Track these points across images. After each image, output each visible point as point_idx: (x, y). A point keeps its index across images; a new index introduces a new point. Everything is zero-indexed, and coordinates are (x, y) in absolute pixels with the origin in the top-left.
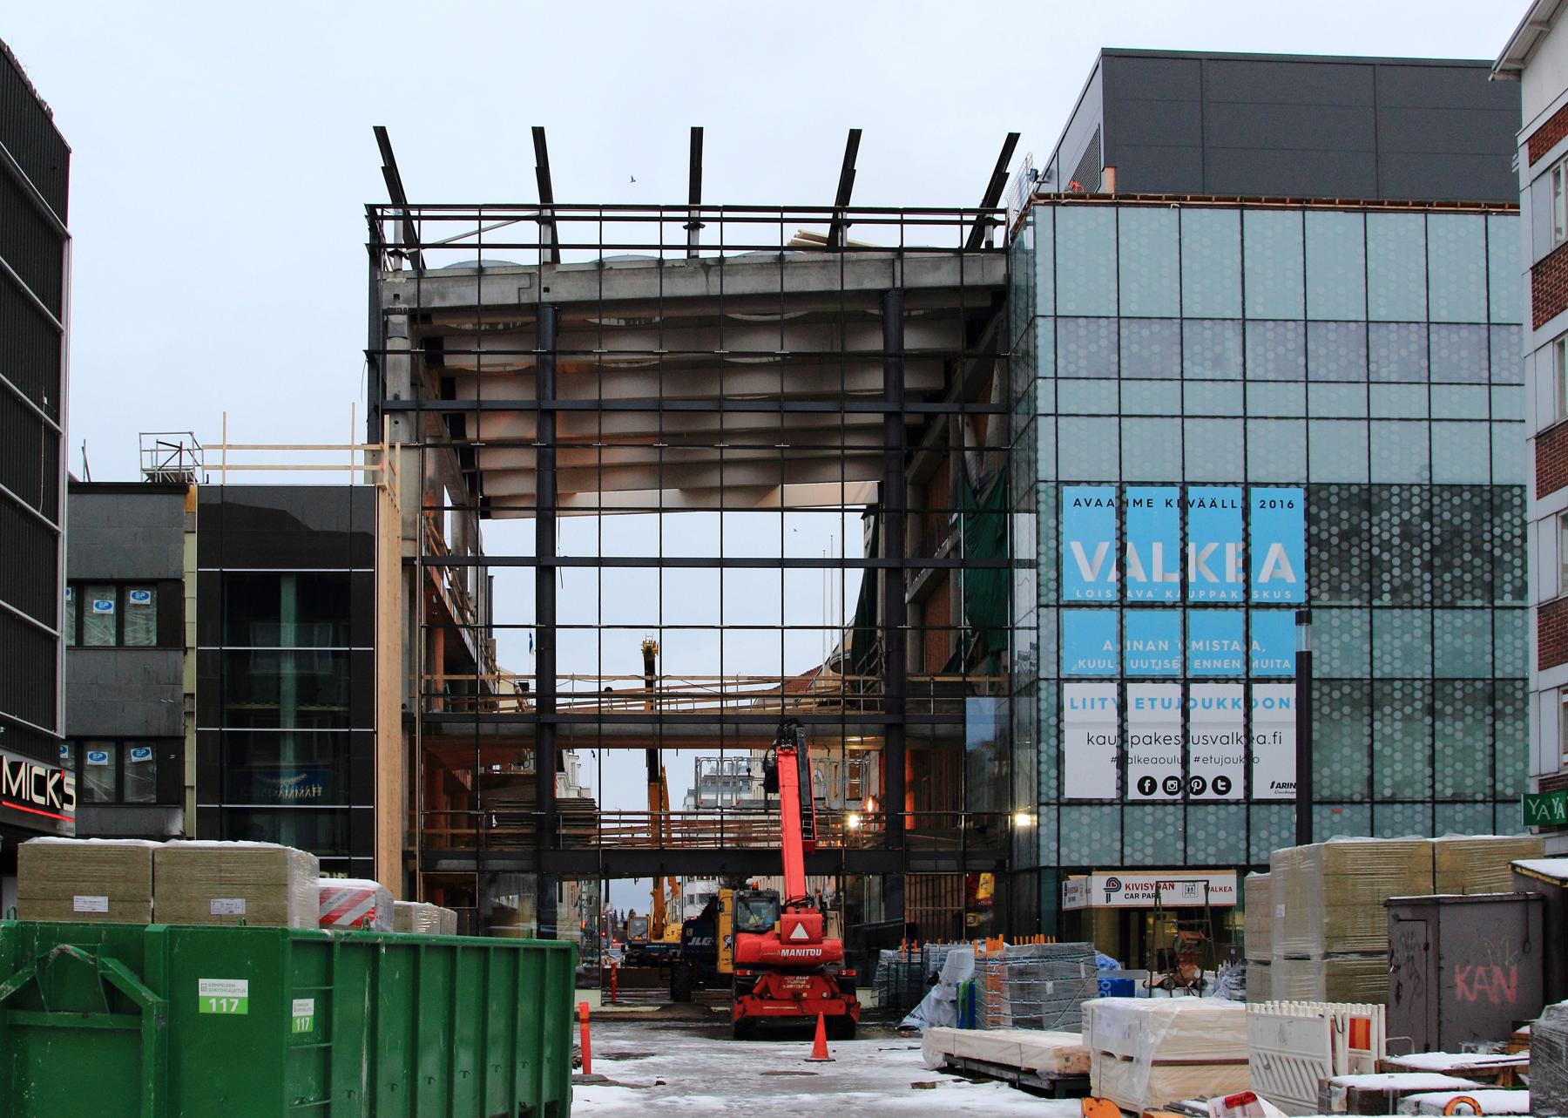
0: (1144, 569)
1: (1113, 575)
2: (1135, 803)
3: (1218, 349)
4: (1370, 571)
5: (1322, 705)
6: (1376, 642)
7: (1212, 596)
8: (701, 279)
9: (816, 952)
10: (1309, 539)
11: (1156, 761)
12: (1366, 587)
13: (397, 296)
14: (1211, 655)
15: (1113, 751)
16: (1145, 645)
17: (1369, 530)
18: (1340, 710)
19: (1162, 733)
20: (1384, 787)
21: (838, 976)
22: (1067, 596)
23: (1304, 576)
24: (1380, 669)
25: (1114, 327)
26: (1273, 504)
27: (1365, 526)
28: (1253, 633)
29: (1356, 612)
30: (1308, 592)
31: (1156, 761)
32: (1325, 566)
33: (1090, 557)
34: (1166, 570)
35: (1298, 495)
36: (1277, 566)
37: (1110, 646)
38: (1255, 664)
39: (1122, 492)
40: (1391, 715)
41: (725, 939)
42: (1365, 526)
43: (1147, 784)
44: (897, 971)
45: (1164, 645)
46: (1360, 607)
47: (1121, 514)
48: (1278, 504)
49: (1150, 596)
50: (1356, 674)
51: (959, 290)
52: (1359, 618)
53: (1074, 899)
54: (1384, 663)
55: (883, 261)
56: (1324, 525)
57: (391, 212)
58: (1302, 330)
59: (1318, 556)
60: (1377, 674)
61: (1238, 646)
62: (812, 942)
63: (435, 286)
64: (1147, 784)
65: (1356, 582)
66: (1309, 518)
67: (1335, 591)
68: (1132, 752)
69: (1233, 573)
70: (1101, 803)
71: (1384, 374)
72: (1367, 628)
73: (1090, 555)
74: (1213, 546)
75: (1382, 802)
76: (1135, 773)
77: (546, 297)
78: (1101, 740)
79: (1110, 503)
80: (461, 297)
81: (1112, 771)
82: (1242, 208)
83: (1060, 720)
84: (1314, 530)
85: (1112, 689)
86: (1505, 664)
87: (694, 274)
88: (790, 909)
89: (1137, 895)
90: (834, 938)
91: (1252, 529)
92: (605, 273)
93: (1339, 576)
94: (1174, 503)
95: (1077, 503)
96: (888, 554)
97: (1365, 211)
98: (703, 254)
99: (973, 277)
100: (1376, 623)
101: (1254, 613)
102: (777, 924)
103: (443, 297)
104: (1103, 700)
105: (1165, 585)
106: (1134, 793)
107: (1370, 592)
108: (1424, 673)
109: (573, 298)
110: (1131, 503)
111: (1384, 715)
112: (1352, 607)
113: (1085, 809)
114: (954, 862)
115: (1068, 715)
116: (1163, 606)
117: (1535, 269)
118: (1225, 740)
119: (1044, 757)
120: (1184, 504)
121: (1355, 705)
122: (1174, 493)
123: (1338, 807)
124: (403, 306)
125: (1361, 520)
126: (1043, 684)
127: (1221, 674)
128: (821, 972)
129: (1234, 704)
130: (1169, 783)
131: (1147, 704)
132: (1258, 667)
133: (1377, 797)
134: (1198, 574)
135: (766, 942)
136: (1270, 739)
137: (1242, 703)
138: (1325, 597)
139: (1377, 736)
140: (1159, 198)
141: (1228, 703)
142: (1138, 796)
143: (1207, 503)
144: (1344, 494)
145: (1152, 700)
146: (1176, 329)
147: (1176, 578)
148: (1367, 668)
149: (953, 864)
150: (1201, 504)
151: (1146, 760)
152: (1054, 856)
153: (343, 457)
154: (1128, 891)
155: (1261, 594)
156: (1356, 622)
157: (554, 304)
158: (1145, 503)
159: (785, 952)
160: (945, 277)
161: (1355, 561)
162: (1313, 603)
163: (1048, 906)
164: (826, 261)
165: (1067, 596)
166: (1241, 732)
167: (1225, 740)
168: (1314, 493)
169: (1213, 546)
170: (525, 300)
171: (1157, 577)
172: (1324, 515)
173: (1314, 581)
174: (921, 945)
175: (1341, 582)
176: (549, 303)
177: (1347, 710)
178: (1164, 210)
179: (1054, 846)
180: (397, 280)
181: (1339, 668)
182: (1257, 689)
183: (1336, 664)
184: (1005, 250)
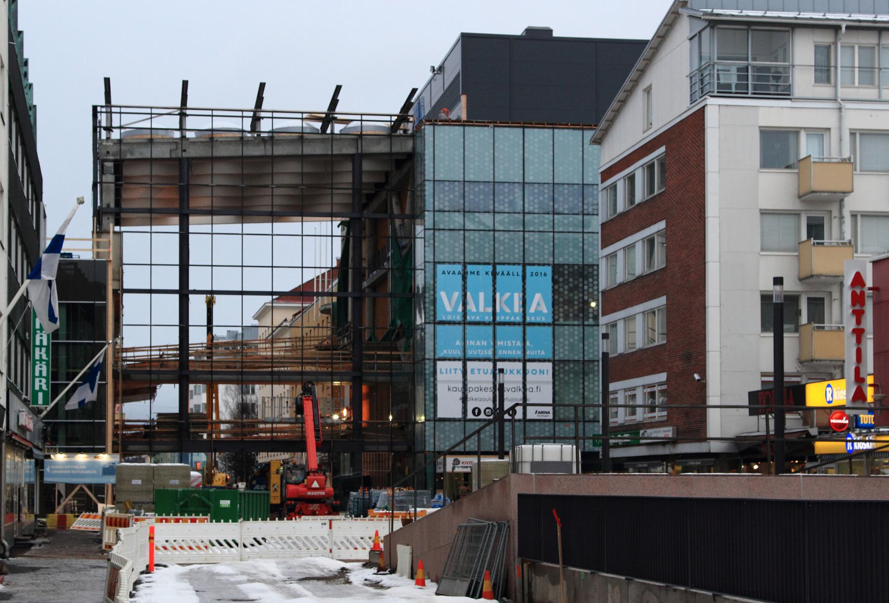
0: (475, 303)
1: (460, 309)
2: (471, 420)
3: (511, 198)
4: (583, 307)
5: (560, 373)
6: (586, 342)
7: (507, 319)
8: (262, 147)
9: (322, 493)
10: (554, 291)
11: (481, 400)
12: (581, 315)
13: (108, 152)
14: (507, 348)
15: (460, 395)
16: (476, 343)
17: (583, 287)
18: (568, 376)
19: (483, 386)
20: (590, 414)
21: (332, 504)
22: (438, 319)
23: (551, 309)
24: (588, 356)
25: (462, 186)
26: (537, 274)
27: (581, 285)
28: (527, 337)
29: (576, 328)
30: (553, 317)
31: (481, 400)
32: (561, 305)
33: (449, 299)
34: (486, 306)
35: (549, 270)
36: (538, 305)
37: (459, 343)
38: (528, 353)
39: (465, 267)
40: (593, 378)
41: (273, 486)
42: (581, 285)
43: (476, 411)
44: (358, 502)
45: (484, 343)
46: (578, 325)
47: (464, 278)
48: (539, 274)
49: (478, 319)
50: (576, 358)
51: (390, 154)
52: (577, 331)
54: (589, 353)
55: (353, 139)
56: (561, 285)
57: (104, 110)
58: (551, 189)
59: (558, 300)
60: (586, 358)
61: (519, 344)
62: (321, 488)
63: (128, 147)
64: (476, 411)
65: (576, 313)
66: (554, 281)
67: (566, 317)
68: (469, 395)
69: (517, 308)
70: (454, 420)
72: (581, 335)
73: (449, 299)
74: (508, 295)
75: (589, 421)
76: (471, 406)
77: (185, 155)
78: (455, 389)
79: (459, 273)
80: (141, 154)
81: (460, 404)
82: (524, 127)
83: (435, 379)
84: (556, 287)
85: (459, 364)
87: (258, 144)
88: (311, 474)
90: (329, 486)
91: (527, 286)
92: (214, 143)
94: (490, 273)
95: (444, 273)
96: (353, 290)
97: (583, 129)
98: (262, 135)
99: (396, 149)
100: (586, 333)
101: (528, 328)
102: (306, 480)
103: (132, 153)
104: (456, 370)
105: (485, 313)
106: (470, 416)
107: (583, 318)
109: (198, 156)
110: (469, 273)
111: (589, 379)
112: (574, 325)
113: (447, 423)
114: (386, 447)
115: (439, 376)
116: (484, 324)
117: (602, 225)
118: (513, 390)
119: (427, 397)
120: (494, 274)
121: (576, 374)
122: (490, 268)
123: (568, 423)
124: (111, 158)
125: (579, 282)
126: (427, 362)
127: (512, 357)
128: (324, 502)
129: (518, 372)
130: (487, 410)
131: (476, 371)
132: (530, 354)
133: (586, 419)
134: (501, 308)
135: (301, 488)
136: (535, 389)
137: (521, 372)
139: (586, 389)
140: (484, 122)
141: (515, 372)
142: (473, 417)
143: (506, 273)
144: (571, 270)
145: (479, 370)
146: (491, 187)
147: (490, 310)
148: (581, 355)
149: (386, 448)
150: (503, 274)
151: (476, 399)
152: (432, 446)
155: (530, 318)
156: (576, 333)
157: (188, 158)
158: (476, 273)
159: (309, 493)
160: (382, 148)
161: (576, 303)
162: (557, 323)
163: (429, 470)
164: (324, 139)
165: (438, 319)
166: (521, 386)
167: (513, 390)
168: (557, 269)
169: (508, 295)
170: (174, 156)
171: (481, 309)
172: (561, 279)
173: (556, 312)
174: (369, 490)
177: (572, 376)
178: (486, 128)
179: (432, 441)
180: (108, 144)
181: (568, 355)
182: (529, 365)
184: (413, 136)
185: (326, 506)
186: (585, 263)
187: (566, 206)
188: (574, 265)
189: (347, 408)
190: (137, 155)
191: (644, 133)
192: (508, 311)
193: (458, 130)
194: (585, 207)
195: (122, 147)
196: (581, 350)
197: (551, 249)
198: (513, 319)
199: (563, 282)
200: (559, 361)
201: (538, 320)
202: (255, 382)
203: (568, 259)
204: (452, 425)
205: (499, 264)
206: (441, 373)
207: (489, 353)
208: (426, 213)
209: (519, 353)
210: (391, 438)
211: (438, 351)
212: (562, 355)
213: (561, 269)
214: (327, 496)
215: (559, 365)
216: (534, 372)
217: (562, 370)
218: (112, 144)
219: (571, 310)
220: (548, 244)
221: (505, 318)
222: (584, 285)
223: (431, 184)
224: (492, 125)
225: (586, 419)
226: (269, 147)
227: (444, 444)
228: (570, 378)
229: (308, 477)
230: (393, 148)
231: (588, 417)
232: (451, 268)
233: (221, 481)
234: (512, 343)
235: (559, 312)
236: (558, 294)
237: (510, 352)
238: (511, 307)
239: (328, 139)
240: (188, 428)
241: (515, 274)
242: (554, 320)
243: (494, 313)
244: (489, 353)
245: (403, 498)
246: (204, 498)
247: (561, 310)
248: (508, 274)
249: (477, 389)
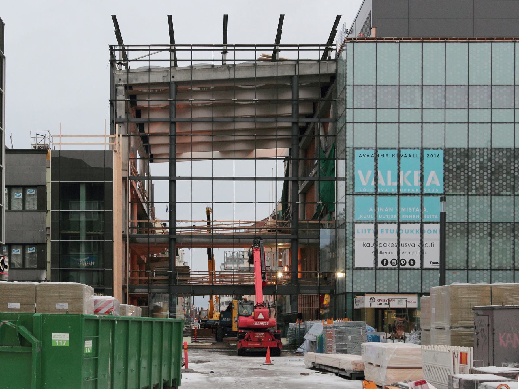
2: (380, 269)
4: (468, 181)
9: (267, 324)
10: (445, 169)
11: (388, 253)
12: (466, 187)
13: (120, 80)
15: (373, 249)
19: (390, 243)
22: (356, 191)
23: (443, 183)
24: (471, 218)
27: (466, 164)
29: (462, 197)
30: (444, 189)
31: (388, 253)
32: (451, 179)
33: (365, 176)
34: (392, 181)
35: (441, 152)
36: (433, 179)
38: (424, 217)
40: (475, 236)
43: (385, 262)
44: (295, 331)
45: (391, 209)
46: (464, 195)
47: (376, 160)
48: (434, 156)
50: (462, 221)
52: (463, 199)
53: (358, 305)
54: (472, 216)
55: (291, 65)
57: (118, 48)
58: (444, 89)
60: (470, 221)
61: (418, 210)
63: (134, 75)
64: (385, 262)
65: (462, 185)
66: (446, 161)
67: (454, 189)
68: (380, 250)
69: (417, 182)
70: (368, 269)
72: (466, 203)
73: (365, 175)
74: (409, 172)
75: (472, 270)
76: (380, 258)
77: (173, 80)
81: (372, 257)
83: (353, 237)
84: (447, 166)
87: (224, 70)
89: (381, 304)
90: (273, 318)
91: (424, 165)
92: (193, 70)
93: (456, 183)
94: (396, 156)
95: (360, 156)
99: (324, 71)
101: (425, 198)
103: (136, 80)
104: (369, 230)
107: (468, 189)
110: (380, 156)
112: (461, 195)
115: (356, 235)
118: (413, 245)
119: (347, 251)
120: (399, 156)
121: (462, 232)
122: (396, 152)
123: (455, 271)
124: (122, 83)
125: (465, 162)
127: (412, 220)
129: (417, 231)
130: (393, 261)
131: (385, 231)
133: (470, 268)
135: (249, 319)
136: (430, 245)
137: (419, 231)
139: (470, 244)
140: (392, 39)
141: (414, 231)
143: (408, 155)
145: (387, 230)
147: (396, 184)
148: (466, 218)
150: (406, 156)
152: (351, 289)
153: (102, 140)
154: (378, 302)
157: (175, 82)
158: (385, 156)
159: (256, 324)
160: (314, 70)
162: (446, 193)
165: (356, 191)
168: (447, 151)
169: (409, 172)
170: (165, 81)
171: (389, 184)
172: (451, 160)
173: (447, 185)
174: (304, 321)
177: (458, 234)
178: (393, 44)
185: (270, 334)
186: (469, 147)
187: (455, 103)
188: (461, 148)
189: (287, 266)
190: (140, 81)
191: (358, 230)
192: (409, 184)
193: (372, 45)
195: (129, 76)
198: (413, 191)
201: (433, 191)
202: (288, 345)
204: (366, 272)
205: (403, 148)
206: (358, 232)
207: (395, 218)
208: (347, 110)
209: (418, 218)
210: (319, 285)
211: (355, 216)
213: (451, 152)
214: (271, 326)
216: (429, 231)
217: (451, 230)
218: (123, 73)
219: (458, 183)
221: (407, 190)
222: (468, 164)
223: (351, 87)
224: (398, 41)
225: (470, 268)
226: (232, 72)
227: (360, 287)
229: (255, 310)
230: (321, 71)
232: (366, 152)
233: (217, 317)
234: (412, 210)
236: (448, 172)
237: (411, 216)
238: (412, 182)
239: (274, 65)
240: (175, 277)
241: (415, 156)
242: (445, 191)
243: (399, 187)
244: (395, 218)
245: (344, 329)
246: (23, 330)
247: (451, 183)
248: (410, 156)
249: (385, 245)
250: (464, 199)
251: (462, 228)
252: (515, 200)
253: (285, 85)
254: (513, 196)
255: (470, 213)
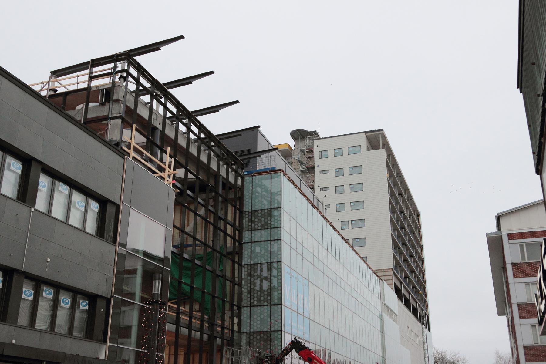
5: (254, 341)
27: (269, 222)
29: (266, 307)
42: (269, 222)
46: (267, 305)
50: (265, 330)
56: (256, 223)
71: (351, 186)
72: (249, 314)
86: (254, 326)
93: (260, 295)
108: (247, 330)
138: (255, 303)
172: (256, 220)
175: (261, 297)
176: (81, 356)
183: (259, 326)
194: (272, 223)
196: (269, 323)
197: (249, 254)
199: (257, 222)
200: (253, 332)
203: (261, 206)
212: (255, 328)
215: (253, 336)
220: (248, 251)
228: (261, 345)
231: (274, 301)
235: (254, 297)
250: (267, 309)
251: (265, 337)
252: (251, 311)
253: (183, 118)
254: (270, 306)
255: (252, 323)
